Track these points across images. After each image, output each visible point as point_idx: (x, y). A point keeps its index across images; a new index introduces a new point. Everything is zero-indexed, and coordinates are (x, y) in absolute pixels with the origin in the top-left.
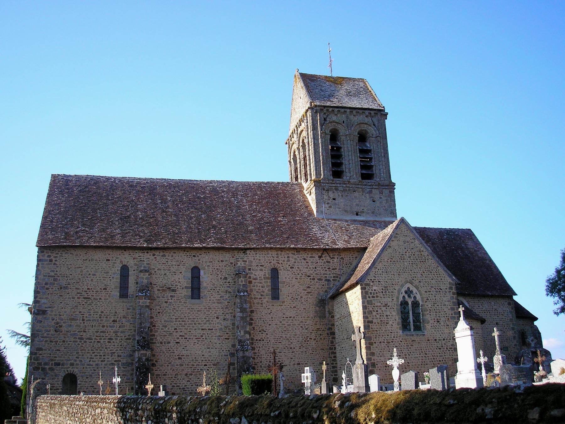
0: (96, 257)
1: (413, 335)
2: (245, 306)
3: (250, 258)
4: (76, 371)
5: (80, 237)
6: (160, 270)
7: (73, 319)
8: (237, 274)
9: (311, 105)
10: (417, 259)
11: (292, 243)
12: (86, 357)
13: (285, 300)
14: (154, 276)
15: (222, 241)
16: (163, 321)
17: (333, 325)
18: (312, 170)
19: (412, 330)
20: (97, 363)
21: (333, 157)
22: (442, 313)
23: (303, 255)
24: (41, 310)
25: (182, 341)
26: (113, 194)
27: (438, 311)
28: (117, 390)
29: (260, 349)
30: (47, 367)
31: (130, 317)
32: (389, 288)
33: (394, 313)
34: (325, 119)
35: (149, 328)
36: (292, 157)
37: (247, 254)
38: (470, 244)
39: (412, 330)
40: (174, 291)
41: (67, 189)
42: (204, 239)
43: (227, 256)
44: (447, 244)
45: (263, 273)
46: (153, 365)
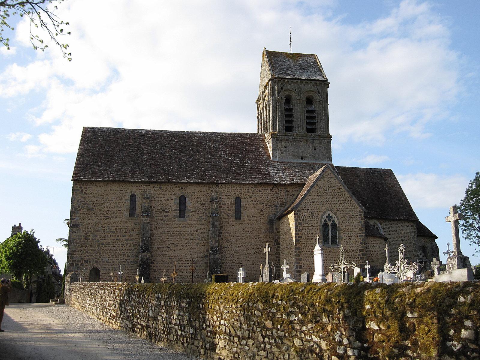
0: (113, 188)
1: (330, 247)
2: (216, 223)
3: (221, 190)
4: (99, 266)
5: (102, 174)
6: (158, 197)
7: (97, 231)
8: (211, 201)
9: (272, 77)
10: (336, 194)
11: (252, 180)
12: (106, 257)
13: (245, 219)
14: (153, 202)
15: (202, 178)
16: (159, 233)
17: (279, 238)
18: (271, 126)
19: (330, 244)
20: (113, 261)
21: (286, 116)
22: (353, 232)
23: (259, 188)
24: (76, 225)
25: (172, 247)
26: (127, 142)
27: (350, 231)
28: (121, 280)
29: (226, 254)
30: (79, 263)
31: (136, 230)
32: (315, 214)
33: (317, 232)
34: (282, 88)
35: (149, 237)
36: (259, 114)
37: (219, 187)
38: (389, 181)
39: (330, 244)
40: (167, 212)
41: (94, 138)
42: (189, 176)
43: (205, 189)
44: (371, 180)
45: (230, 201)
46: (152, 263)
